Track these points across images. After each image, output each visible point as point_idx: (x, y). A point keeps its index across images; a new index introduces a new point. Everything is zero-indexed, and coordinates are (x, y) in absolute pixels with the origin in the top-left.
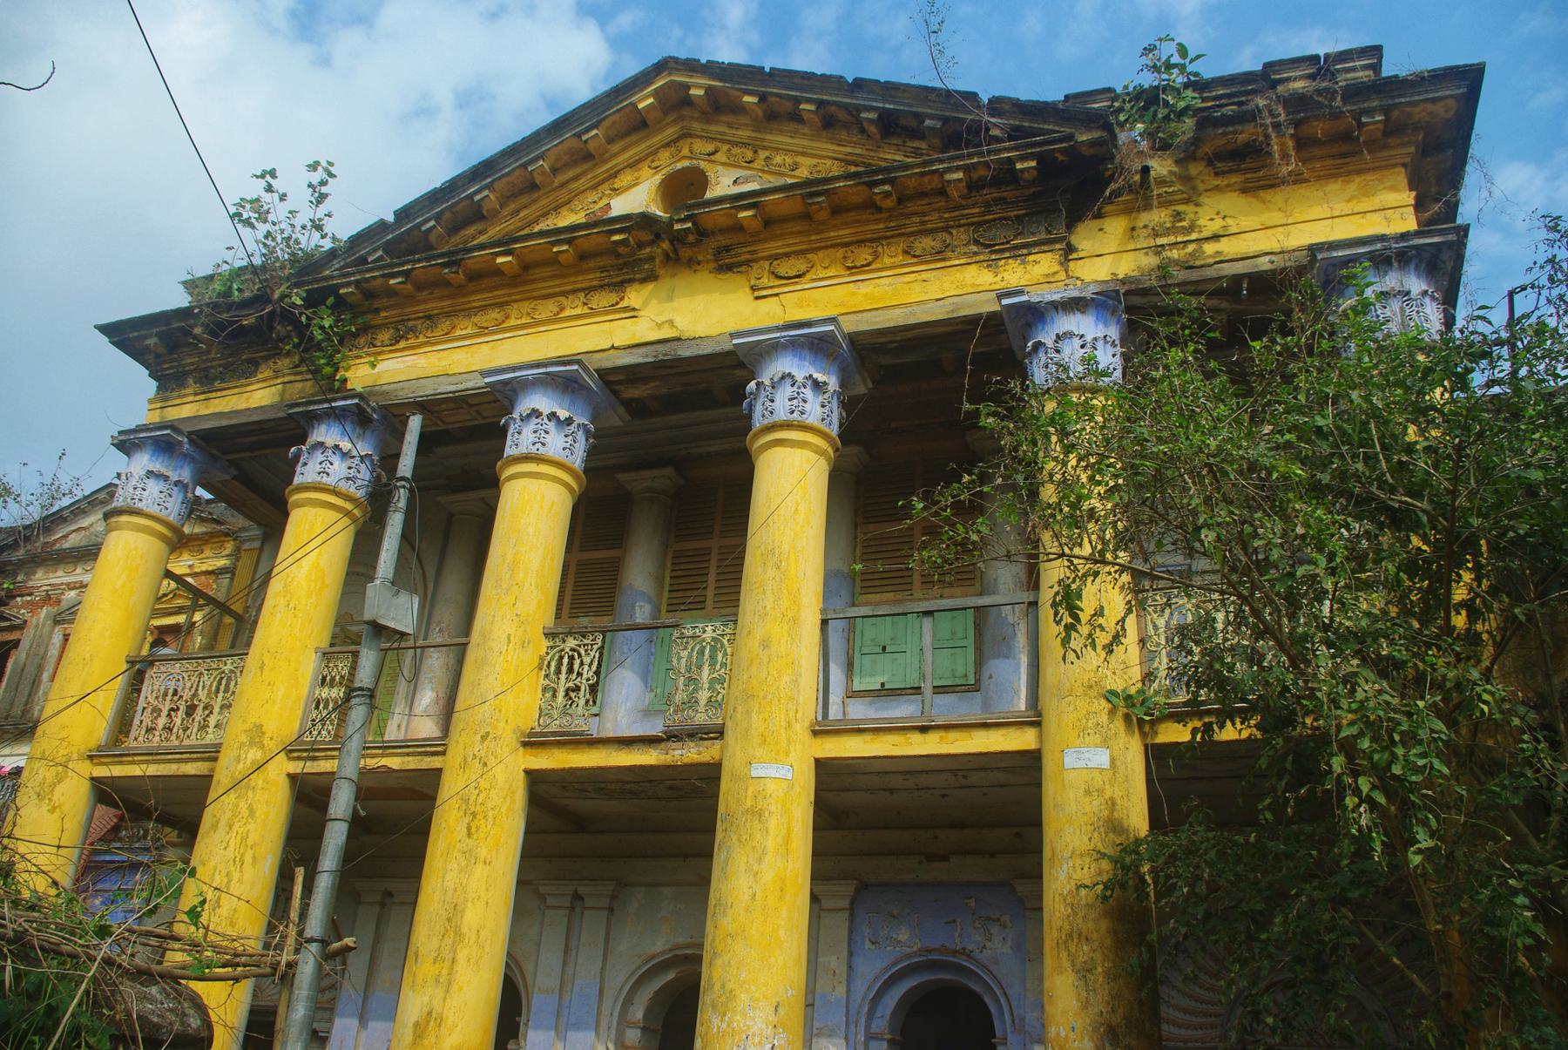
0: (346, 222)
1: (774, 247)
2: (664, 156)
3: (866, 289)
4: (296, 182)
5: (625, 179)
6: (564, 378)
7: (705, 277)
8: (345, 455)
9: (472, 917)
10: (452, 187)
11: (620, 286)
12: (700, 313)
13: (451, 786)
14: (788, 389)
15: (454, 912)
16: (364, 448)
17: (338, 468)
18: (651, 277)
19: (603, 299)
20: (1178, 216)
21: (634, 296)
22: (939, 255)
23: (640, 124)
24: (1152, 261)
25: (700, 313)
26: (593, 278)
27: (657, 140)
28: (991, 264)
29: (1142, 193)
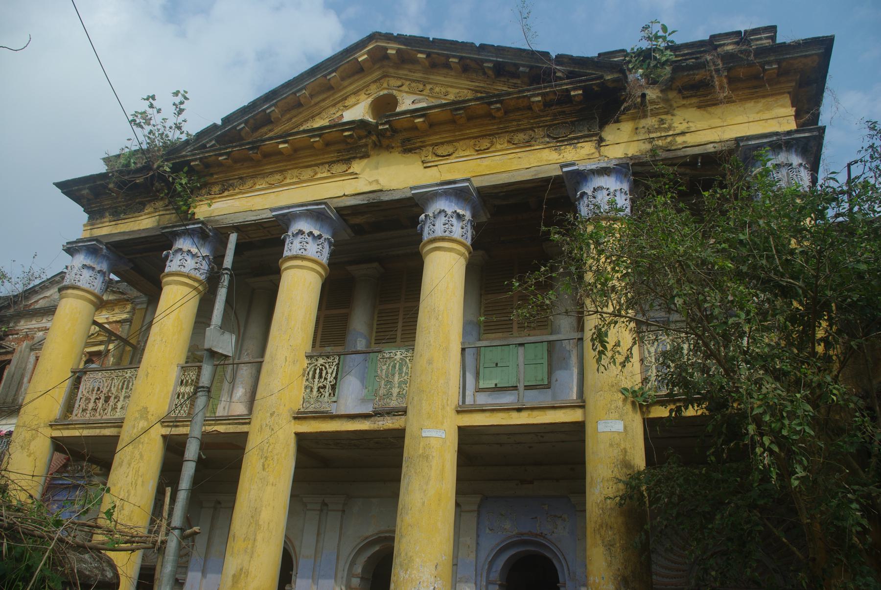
0: (195, 124)
1: (435, 139)
2: (373, 87)
3: (486, 162)
4: (166, 102)
5: (351, 100)
6: (317, 212)
7: (396, 156)
8: (194, 256)
9: (265, 515)
10: (254, 105)
11: (348, 161)
12: (392, 176)
13: (253, 443)
14: (442, 219)
15: (255, 513)
16: (205, 252)
17: (190, 263)
18: (366, 156)
19: (339, 168)
20: (662, 121)
21: (356, 166)
22: (528, 143)
23: (360, 70)
24: (647, 146)
25: (392, 176)
26: (333, 156)
27: (369, 79)
28: (557, 149)
29: (641, 109)
